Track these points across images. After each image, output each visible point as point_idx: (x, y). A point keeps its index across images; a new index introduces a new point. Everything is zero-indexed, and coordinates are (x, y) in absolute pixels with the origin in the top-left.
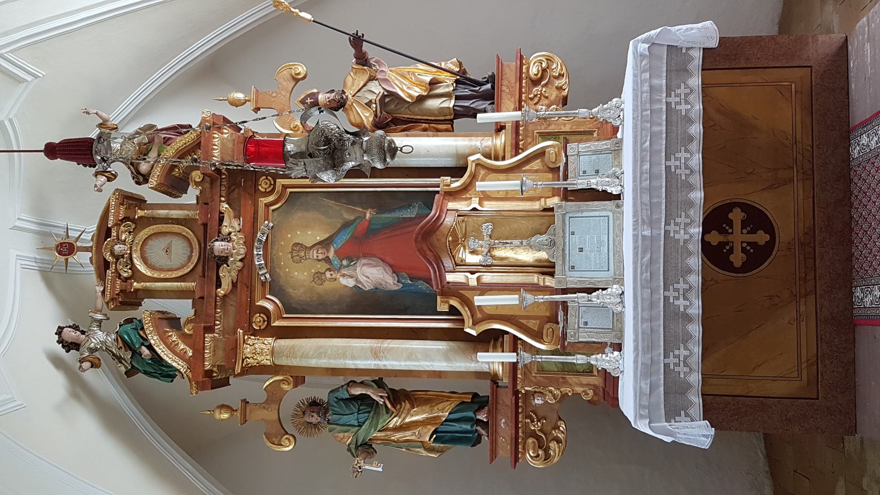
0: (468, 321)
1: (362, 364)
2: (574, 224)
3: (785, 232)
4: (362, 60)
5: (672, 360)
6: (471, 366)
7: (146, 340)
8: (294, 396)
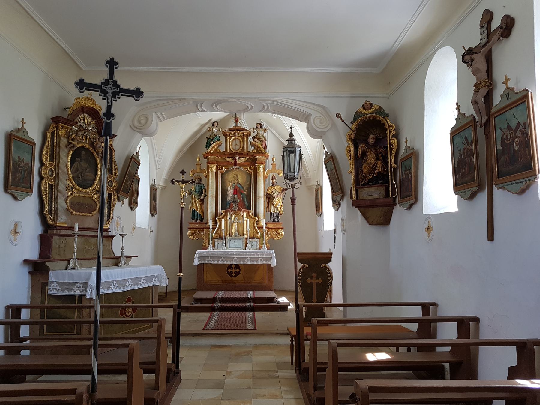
0: (219, 217)
1: (210, 192)
2: (240, 240)
3: (234, 279)
4: (283, 190)
5: (210, 258)
6: (209, 218)
7: (215, 142)
8: (203, 175)
